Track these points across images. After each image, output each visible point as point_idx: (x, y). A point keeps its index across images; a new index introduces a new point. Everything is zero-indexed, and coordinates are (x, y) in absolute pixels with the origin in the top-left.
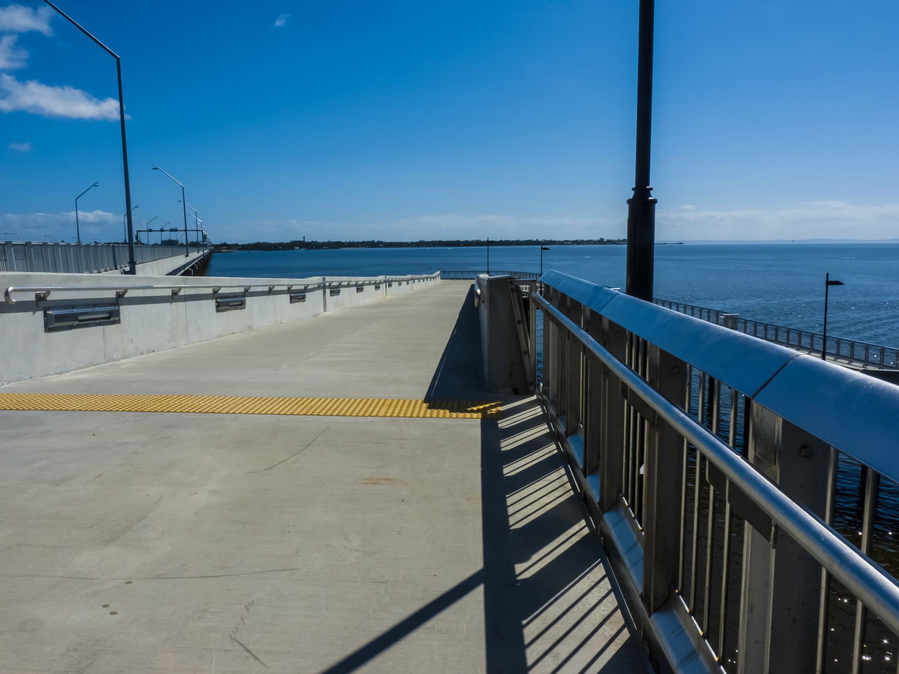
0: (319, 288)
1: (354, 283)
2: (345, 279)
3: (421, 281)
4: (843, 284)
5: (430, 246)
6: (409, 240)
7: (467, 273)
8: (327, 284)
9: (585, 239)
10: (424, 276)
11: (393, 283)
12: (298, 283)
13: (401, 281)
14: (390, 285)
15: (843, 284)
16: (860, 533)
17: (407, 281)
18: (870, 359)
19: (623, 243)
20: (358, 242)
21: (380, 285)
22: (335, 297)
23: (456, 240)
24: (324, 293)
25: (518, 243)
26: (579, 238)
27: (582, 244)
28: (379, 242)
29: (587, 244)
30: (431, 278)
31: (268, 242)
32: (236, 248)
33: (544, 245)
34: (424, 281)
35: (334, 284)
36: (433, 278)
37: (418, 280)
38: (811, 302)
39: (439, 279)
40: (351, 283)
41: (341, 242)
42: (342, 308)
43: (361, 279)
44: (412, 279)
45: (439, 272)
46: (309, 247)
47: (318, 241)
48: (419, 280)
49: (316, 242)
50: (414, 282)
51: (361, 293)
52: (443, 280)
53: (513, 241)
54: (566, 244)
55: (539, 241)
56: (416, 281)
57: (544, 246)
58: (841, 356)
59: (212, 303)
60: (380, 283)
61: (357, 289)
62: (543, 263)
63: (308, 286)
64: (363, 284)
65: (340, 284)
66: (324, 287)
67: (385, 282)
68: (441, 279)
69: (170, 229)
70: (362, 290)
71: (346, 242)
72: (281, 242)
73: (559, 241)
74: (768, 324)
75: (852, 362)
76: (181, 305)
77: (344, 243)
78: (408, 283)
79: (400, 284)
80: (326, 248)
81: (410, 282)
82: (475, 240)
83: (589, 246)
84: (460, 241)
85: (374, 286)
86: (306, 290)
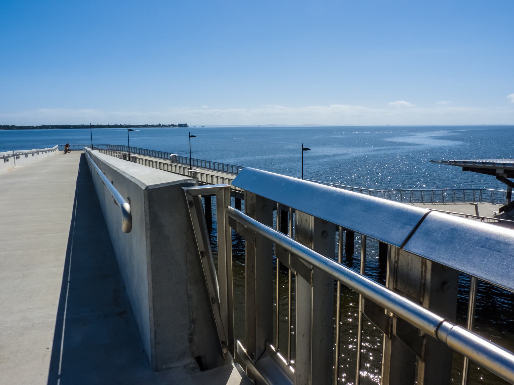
3: (44, 153)
4: (310, 150)
5: (50, 128)
6: (35, 125)
8: (15, 154)
9: (150, 124)
10: (46, 149)
11: (29, 155)
15: (310, 150)
17: (33, 154)
18: (199, 165)
21: (9, 158)
25: (109, 126)
26: (146, 124)
27: (148, 127)
29: (151, 127)
30: (51, 150)
33: (129, 128)
34: (46, 153)
36: (53, 150)
38: (449, 164)
39: (57, 150)
44: (36, 152)
45: (57, 146)
51: (19, 159)
53: (105, 125)
54: (139, 127)
56: (40, 153)
57: (129, 129)
60: (8, 157)
62: (129, 138)
64: (19, 154)
67: (13, 155)
68: (59, 150)
69: (507, 198)
79: (43, 153)
81: (35, 154)
82: (80, 124)
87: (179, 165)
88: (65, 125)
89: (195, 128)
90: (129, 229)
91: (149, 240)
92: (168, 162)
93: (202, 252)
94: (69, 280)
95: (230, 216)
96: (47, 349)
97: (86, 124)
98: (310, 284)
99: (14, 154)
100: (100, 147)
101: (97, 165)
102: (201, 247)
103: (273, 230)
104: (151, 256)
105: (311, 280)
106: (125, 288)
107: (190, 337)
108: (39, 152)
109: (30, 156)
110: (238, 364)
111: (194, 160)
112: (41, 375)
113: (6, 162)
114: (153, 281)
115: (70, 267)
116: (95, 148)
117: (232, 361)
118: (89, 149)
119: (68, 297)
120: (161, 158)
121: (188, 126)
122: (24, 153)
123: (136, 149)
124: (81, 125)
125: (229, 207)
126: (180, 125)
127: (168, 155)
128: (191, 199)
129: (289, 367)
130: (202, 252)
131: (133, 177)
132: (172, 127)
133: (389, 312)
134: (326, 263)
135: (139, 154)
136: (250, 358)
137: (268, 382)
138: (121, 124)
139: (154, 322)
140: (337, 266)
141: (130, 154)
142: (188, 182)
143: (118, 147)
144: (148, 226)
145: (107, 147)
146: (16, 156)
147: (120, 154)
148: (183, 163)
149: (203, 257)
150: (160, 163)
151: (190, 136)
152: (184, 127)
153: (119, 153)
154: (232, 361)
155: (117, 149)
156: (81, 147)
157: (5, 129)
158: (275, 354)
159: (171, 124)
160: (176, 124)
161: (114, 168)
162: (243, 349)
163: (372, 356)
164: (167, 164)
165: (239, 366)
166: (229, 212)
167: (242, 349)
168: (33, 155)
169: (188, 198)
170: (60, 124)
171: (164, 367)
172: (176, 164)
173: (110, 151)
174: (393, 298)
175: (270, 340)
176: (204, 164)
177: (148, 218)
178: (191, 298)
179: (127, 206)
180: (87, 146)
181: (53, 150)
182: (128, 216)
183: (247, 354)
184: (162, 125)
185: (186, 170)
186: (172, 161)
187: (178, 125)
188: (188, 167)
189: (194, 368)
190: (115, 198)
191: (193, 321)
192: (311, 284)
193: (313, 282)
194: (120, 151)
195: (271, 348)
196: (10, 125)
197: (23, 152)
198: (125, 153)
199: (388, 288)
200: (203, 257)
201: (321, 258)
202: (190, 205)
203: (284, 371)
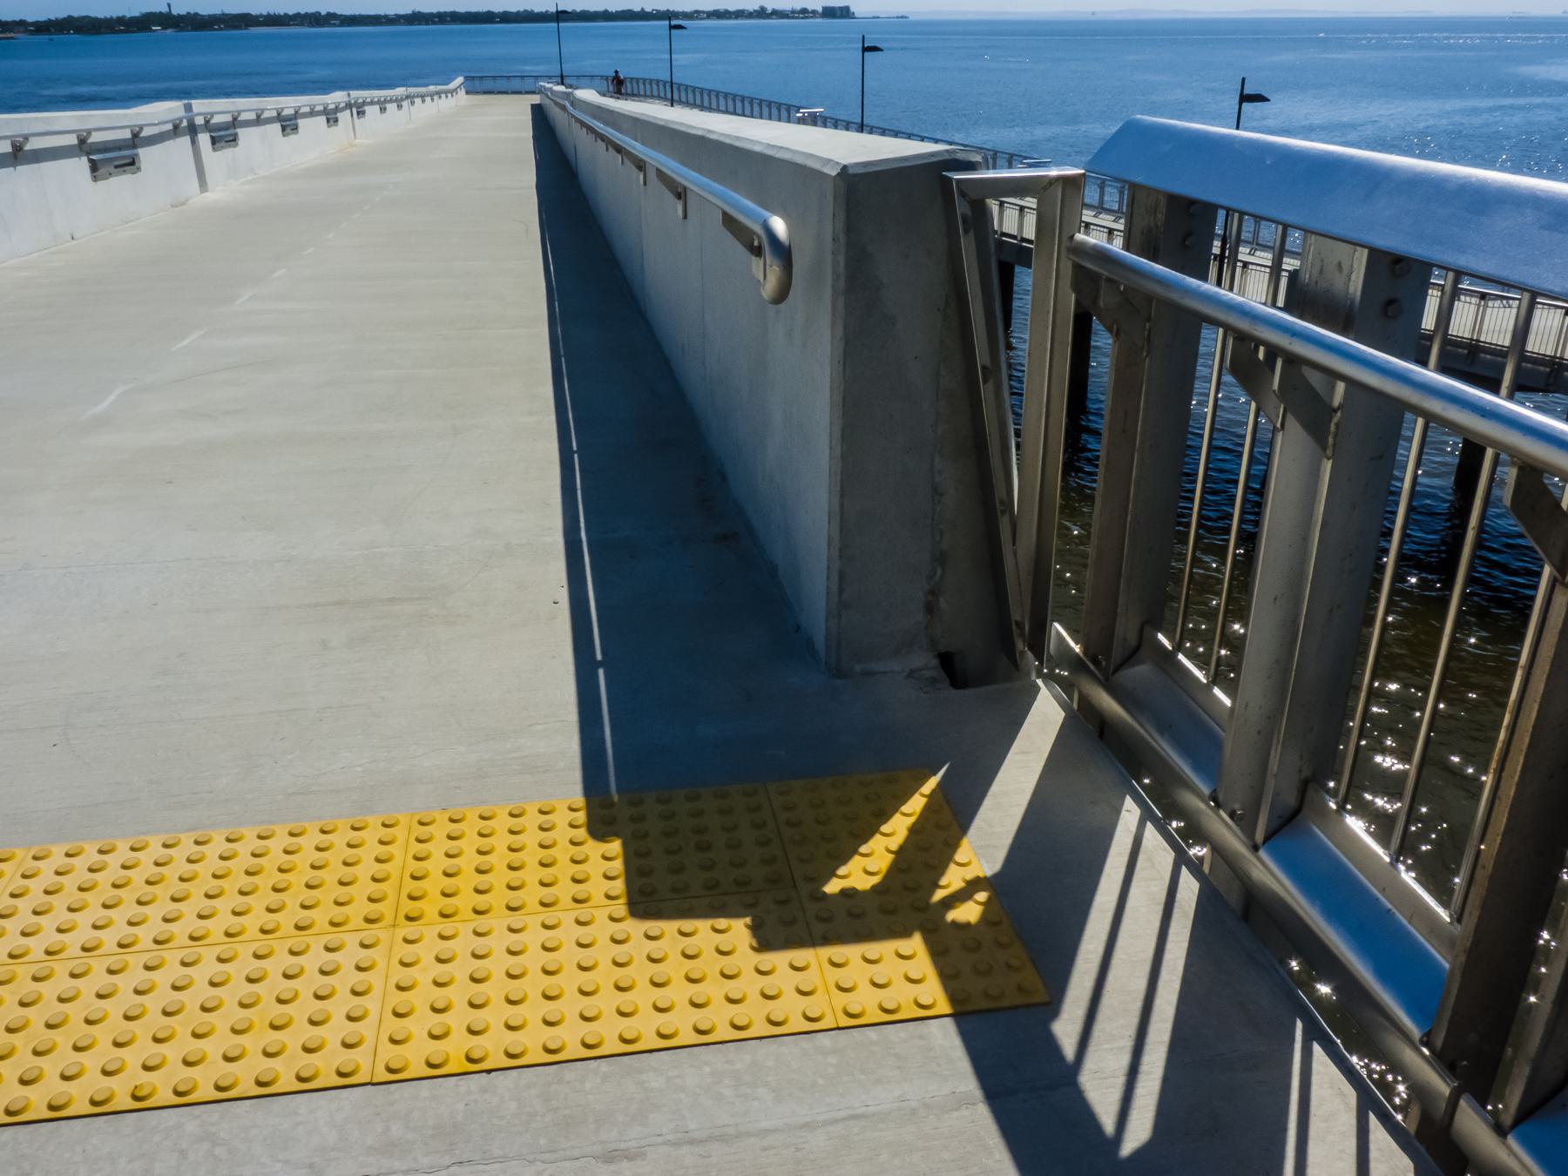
0: (176, 131)
1: (274, 114)
2: (246, 105)
3: (428, 99)
4: (1268, 100)
5: (434, 23)
7: (518, 80)
9: (732, 8)
10: (432, 88)
11: (367, 108)
12: (108, 123)
13: (386, 101)
14: (361, 113)
15: (1268, 100)
16: (1351, 724)
19: (801, 16)
20: (286, 15)
21: (339, 115)
22: (227, 153)
23: (485, 10)
24: (194, 142)
25: (606, 16)
28: (329, 14)
29: (736, 18)
30: (446, 92)
31: (92, 14)
32: (22, 29)
34: (432, 100)
35: (217, 119)
37: (377, 108)
40: (266, 115)
41: (248, 14)
42: (250, 177)
43: (289, 103)
44: (407, 97)
45: (460, 80)
46: (182, 25)
47: (200, 13)
49: (196, 14)
50: (413, 103)
51: (335, 128)
52: (470, 96)
54: (697, 18)
55: (647, 12)
58: (1261, 245)
59: (82, 163)
60: (337, 109)
61: (284, 128)
63: (239, 114)
64: (297, 115)
65: (235, 119)
66: (193, 130)
67: (349, 106)
68: (467, 93)
70: (295, 129)
71: (261, 16)
72: (120, 15)
73: (683, 12)
75: (1101, 213)
76: (23, 169)
77: (257, 17)
78: (400, 107)
79: (383, 110)
80: (220, 29)
81: (405, 104)
82: (521, 10)
83: (739, 21)
84: (493, 13)
85: (323, 118)
86: (137, 140)
88: (476, 10)
94: (575, 449)
95: (1078, 260)
96: (555, 603)
98: (1324, 449)
99: (350, 101)
103: (1228, 295)
104: (844, 370)
105: (1331, 440)
106: (724, 477)
107: (930, 598)
108: (414, 97)
113: (332, 126)
114: (843, 437)
121: (853, 13)
123: (694, 92)
124: (525, 11)
126: (829, 13)
127: (792, 112)
131: (781, 148)
132: (802, 18)
138: (643, 9)
139: (841, 551)
143: (638, 83)
144: (842, 284)
145: (605, 82)
146: (358, 108)
151: (865, 49)
152: (842, 17)
156: (529, 84)
157: (308, 26)
159: (798, 7)
160: (818, 9)
161: (694, 132)
162: (1072, 644)
167: (1067, 645)
171: (858, 668)
175: (1155, 620)
177: (841, 259)
178: (941, 495)
180: (549, 78)
181: (446, 92)
183: (1081, 655)
184: (769, 11)
187: (820, 10)
189: (934, 681)
191: (941, 559)
193: (1334, 445)
195: (1159, 642)
196: (323, 13)
197: (374, 97)
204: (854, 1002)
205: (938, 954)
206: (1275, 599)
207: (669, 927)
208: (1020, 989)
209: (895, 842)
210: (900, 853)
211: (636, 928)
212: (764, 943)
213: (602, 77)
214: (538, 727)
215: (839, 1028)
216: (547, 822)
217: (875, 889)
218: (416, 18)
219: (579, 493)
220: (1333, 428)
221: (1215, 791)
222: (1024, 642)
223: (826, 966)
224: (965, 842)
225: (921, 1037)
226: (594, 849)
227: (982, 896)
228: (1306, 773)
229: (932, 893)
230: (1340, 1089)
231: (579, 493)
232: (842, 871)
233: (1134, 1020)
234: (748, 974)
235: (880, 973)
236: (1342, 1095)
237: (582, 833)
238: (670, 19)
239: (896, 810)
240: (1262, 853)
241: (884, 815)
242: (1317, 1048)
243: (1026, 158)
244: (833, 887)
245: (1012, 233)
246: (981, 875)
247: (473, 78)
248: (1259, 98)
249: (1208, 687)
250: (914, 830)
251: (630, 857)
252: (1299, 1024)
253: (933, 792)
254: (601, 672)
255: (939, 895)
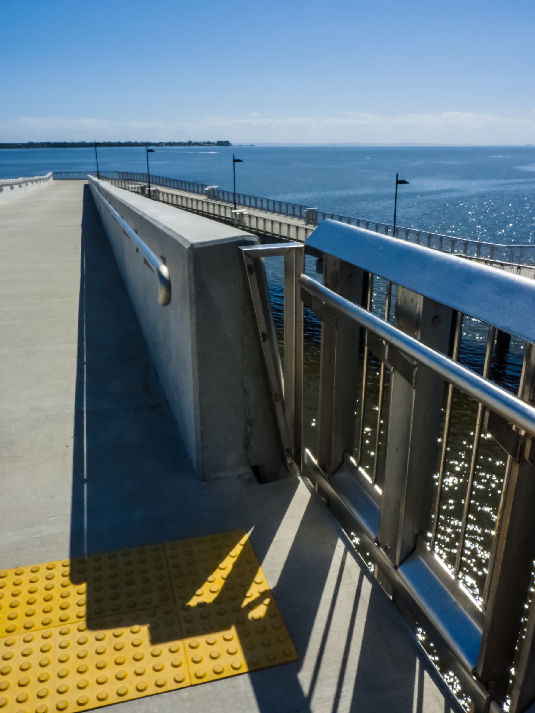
5: (39, 147)
10: (37, 178)
13: (13, 184)
16: (472, 433)
17: (20, 184)
25: (119, 144)
30: (44, 179)
39: (51, 179)
45: (50, 173)
48: (32, 182)
50: (27, 185)
54: (161, 146)
57: (149, 148)
62: (146, 162)
68: (54, 179)
74: (343, 217)
81: (23, 185)
87: (219, 203)
89: (242, 149)
90: (168, 301)
91: (194, 316)
92: (203, 198)
93: (263, 335)
97: (88, 141)
100: (109, 176)
101: (110, 203)
102: (262, 328)
105: (414, 380)
109: (16, 187)
110: (306, 477)
111: (239, 195)
112: (64, 478)
115: (85, 344)
116: (102, 176)
117: (298, 474)
118: (95, 179)
119: (87, 383)
120: (190, 191)
121: (231, 144)
122: (8, 184)
125: (303, 275)
126: (220, 143)
127: (204, 188)
128: (251, 262)
129: (374, 486)
130: (263, 335)
133: (520, 429)
134: (438, 361)
135: (163, 185)
136: (322, 472)
137: (345, 503)
140: (456, 367)
141: (151, 185)
142: (247, 239)
144: (194, 298)
147: (137, 186)
148: (223, 200)
149: (264, 340)
150: (187, 198)
151: (235, 161)
153: (135, 184)
154: (298, 474)
155: (132, 179)
156: (82, 176)
158: (356, 468)
161: (139, 213)
163: (484, 481)
164: (202, 202)
165: (307, 480)
166: (303, 282)
168: (20, 187)
169: (247, 262)
170: (52, 140)
171: (213, 476)
172: (214, 202)
173: (120, 180)
174: (529, 413)
176: (253, 201)
177: (193, 287)
179: (164, 270)
180: (92, 173)
182: (166, 283)
183: (318, 466)
185: (228, 210)
186: (209, 197)
188: (225, 205)
190: (144, 256)
191: (249, 423)
192: (413, 385)
193: (416, 383)
194: (137, 181)
198: (143, 184)
199: (522, 399)
200: (264, 340)
201: (432, 354)
202: (249, 272)
203: (366, 490)
204: (200, 669)
205: (243, 637)
206: (397, 449)
207: (108, 633)
208: (284, 654)
209: (225, 573)
210: (228, 579)
211: (90, 635)
212: (155, 640)
213: (117, 172)
214: (51, 519)
215: (192, 686)
216: (50, 574)
217: (216, 601)
218: (30, 145)
219: (85, 386)
220: (414, 374)
221: (377, 538)
222: (292, 459)
223: (188, 649)
224: (261, 571)
225: (234, 687)
226: (73, 589)
227: (267, 601)
228: (416, 531)
229: (242, 601)
230: (437, 696)
231: (85, 386)
232: (199, 592)
233: (339, 666)
234: (148, 657)
235: (214, 650)
236: (438, 700)
237: (67, 580)
238: (147, 147)
239: (227, 554)
240: (399, 570)
241: (221, 558)
242: (426, 674)
243: (307, 207)
244: (193, 602)
245: (303, 240)
246: (268, 588)
247: (56, 173)
248: (404, 182)
249: (373, 485)
250: (236, 565)
251: (89, 592)
252: (418, 661)
253: (246, 543)
254: (85, 486)
255: (246, 602)
